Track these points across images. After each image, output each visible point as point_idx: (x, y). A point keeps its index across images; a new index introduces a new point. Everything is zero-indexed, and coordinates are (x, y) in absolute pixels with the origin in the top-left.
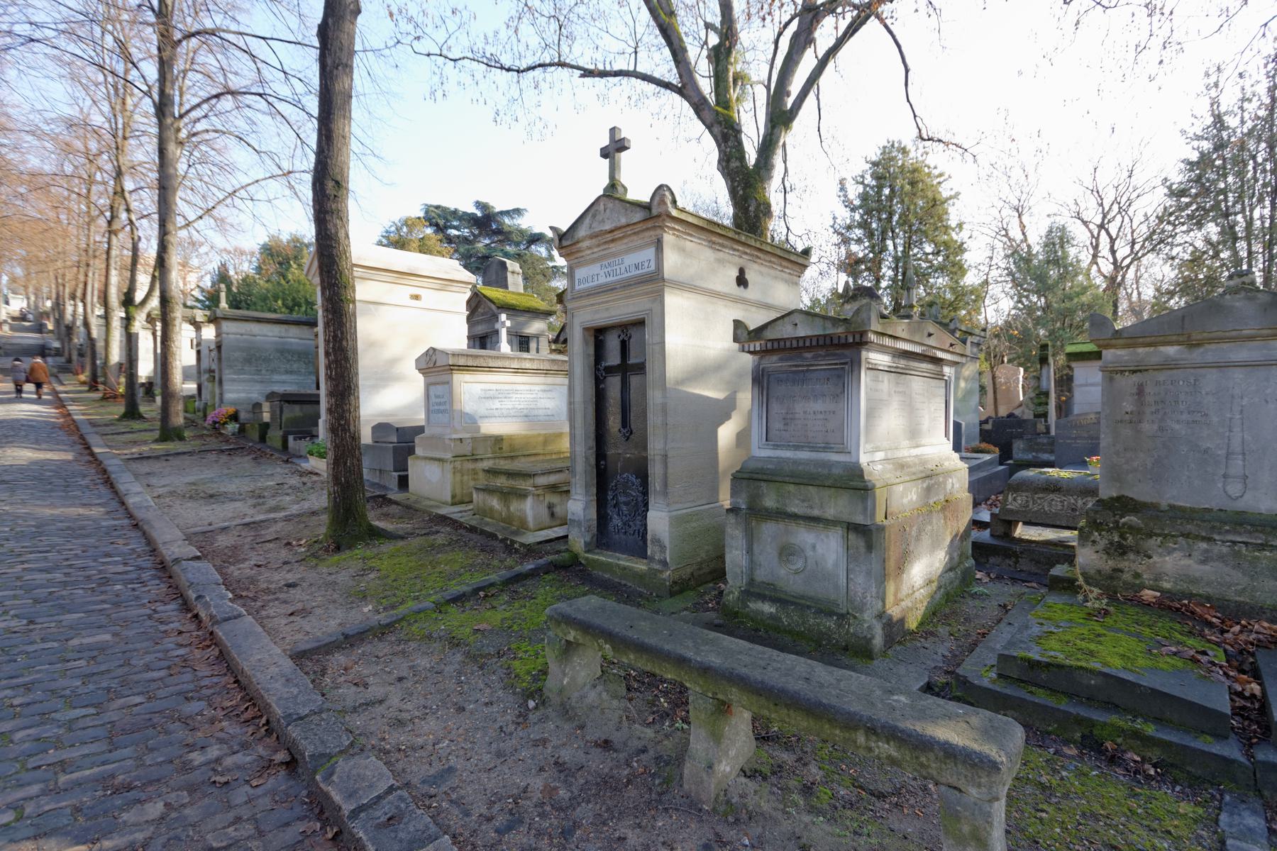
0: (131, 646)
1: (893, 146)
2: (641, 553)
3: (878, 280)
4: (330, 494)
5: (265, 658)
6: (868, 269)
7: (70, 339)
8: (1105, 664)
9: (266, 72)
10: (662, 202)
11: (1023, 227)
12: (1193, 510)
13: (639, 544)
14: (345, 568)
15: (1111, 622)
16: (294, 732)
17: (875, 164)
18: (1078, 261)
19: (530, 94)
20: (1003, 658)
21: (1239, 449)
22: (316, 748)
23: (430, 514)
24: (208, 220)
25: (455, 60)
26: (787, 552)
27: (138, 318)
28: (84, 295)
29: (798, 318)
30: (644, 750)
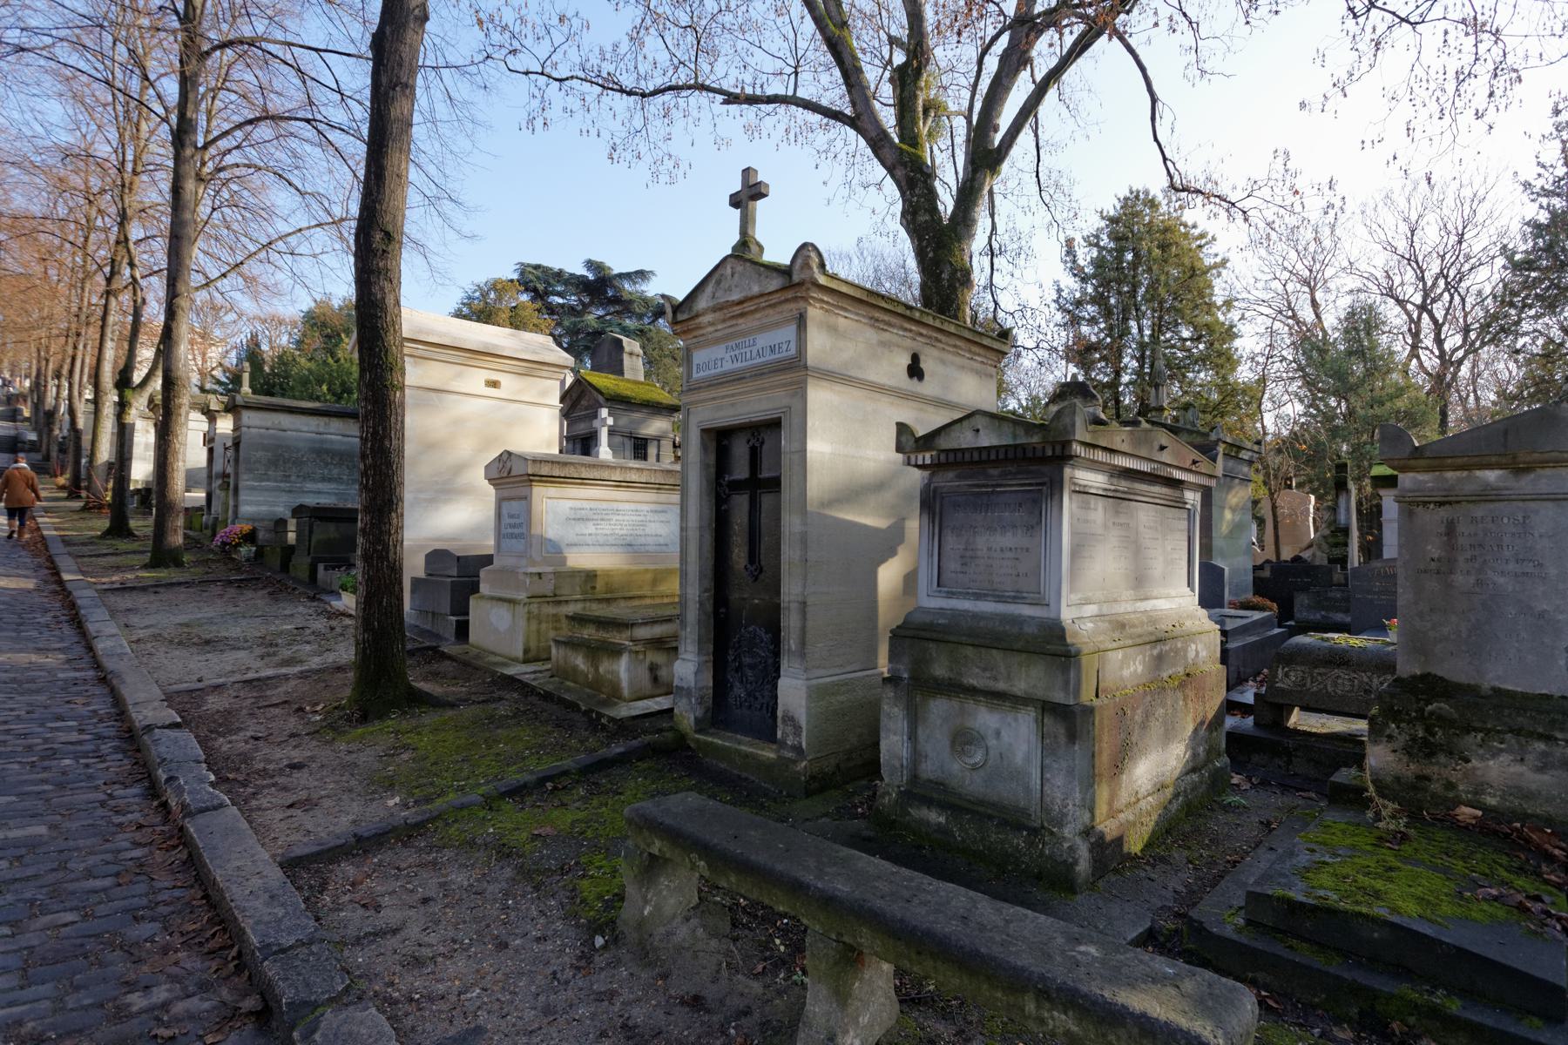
0: (71, 843)
1: (1137, 197)
3: (1118, 374)
4: (357, 644)
5: (247, 866)
6: (1103, 358)
7: (51, 430)
8: (1395, 910)
9: (319, 94)
11: (1314, 304)
12: (1525, 696)
13: (765, 722)
14: (369, 747)
15: (1410, 850)
16: (271, 969)
18: (1392, 353)
19: (657, 127)
20: (1254, 898)
22: (297, 993)
23: (494, 673)
24: (235, 280)
25: (560, 80)
26: (963, 740)
27: (135, 404)
28: (71, 372)
29: (980, 422)
30: (746, 1012)
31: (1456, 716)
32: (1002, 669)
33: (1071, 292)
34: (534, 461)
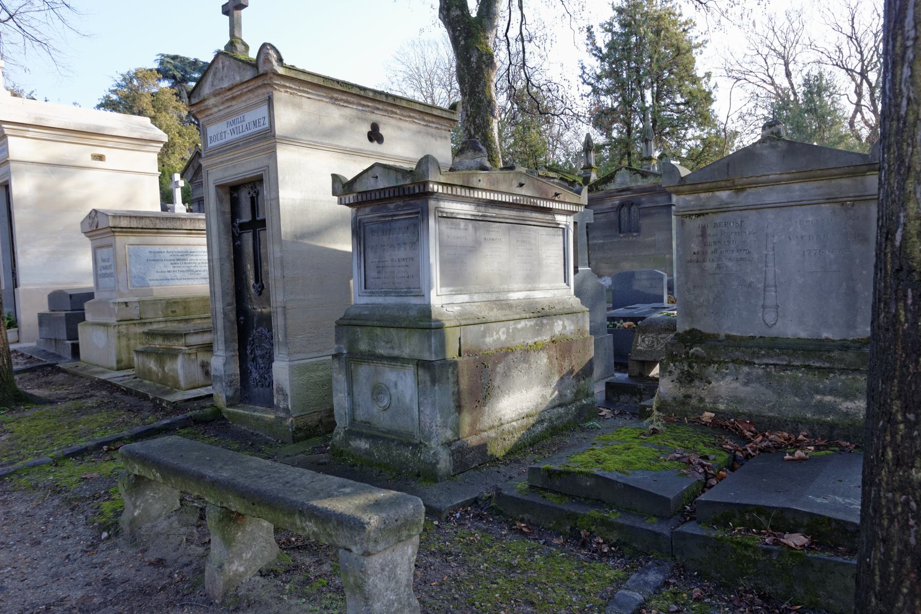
2: (269, 403)
10: (268, 60)
17: (620, 11)
21: (772, 283)
23: (93, 379)
26: (378, 391)
31: (705, 355)
32: (396, 341)
33: (592, 68)
34: (114, 217)
